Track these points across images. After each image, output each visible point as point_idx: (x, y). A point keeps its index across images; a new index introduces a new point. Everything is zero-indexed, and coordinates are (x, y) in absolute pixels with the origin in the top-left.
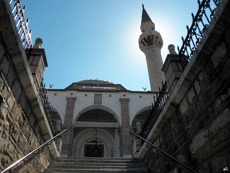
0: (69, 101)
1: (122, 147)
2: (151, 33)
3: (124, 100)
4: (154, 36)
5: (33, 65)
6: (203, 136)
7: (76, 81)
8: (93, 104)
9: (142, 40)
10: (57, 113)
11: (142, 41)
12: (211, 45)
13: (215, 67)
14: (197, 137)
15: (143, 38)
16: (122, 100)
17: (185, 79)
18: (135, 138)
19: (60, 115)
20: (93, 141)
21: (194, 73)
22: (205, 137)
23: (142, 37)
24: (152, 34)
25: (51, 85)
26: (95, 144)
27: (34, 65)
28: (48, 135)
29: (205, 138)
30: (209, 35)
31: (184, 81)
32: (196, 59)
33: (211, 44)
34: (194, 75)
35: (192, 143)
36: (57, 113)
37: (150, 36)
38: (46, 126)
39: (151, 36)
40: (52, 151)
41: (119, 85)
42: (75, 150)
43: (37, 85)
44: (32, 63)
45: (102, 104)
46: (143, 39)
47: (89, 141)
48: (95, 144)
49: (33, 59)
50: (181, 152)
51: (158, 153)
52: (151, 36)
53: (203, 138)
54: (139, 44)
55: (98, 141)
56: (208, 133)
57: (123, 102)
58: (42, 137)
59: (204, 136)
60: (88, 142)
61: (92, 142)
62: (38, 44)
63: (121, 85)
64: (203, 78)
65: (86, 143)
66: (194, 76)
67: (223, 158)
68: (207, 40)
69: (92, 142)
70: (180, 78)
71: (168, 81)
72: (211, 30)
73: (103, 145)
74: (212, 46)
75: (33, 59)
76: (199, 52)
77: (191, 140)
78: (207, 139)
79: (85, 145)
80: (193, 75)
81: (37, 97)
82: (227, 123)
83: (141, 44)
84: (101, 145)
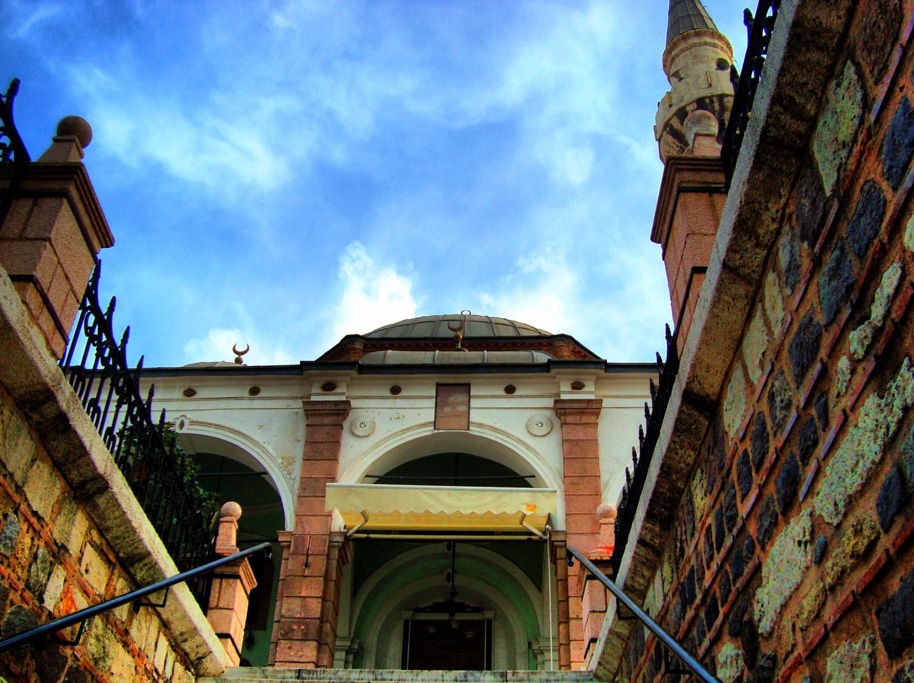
0: (317, 420)
1: (568, 627)
2: (714, 84)
3: (576, 405)
4: (725, 99)
5: (27, 239)
6: (796, 544)
7: (363, 329)
8: (428, 431)
9: (670, 119)
10: (263, 476)
11: (672, 128)
12: (806, 84)
13: (828, 193)
14: (774, 550)
15: (674, 109)
16: (567, 406)
17: (725, 265)
18: (587, 580)
19: (275, 485)
20: (440, 604)
21: (757, 238)
22: (803, 545)
23: (671, 106)
24: (719, 92)
25: (239, 349)
26: (444, 617)
27: (31, 239)
28: (146, 561)
29: (802, 553)
30: (787, 36)
31: (721, 280)
32: (751, 162)
33: (804, 80)
34: (757, 245)
35: (760, 585)
36: (263, 476)
37: (707, 101)
38: (126, 522)
39: (712, 102)
40: (186, 640)
41: (563, 337)
42: (360, 644)
43: (45, 328)
44: (25, 228)
45: (474, 431)
46: (675, 114)
47: (421, 606)
48: (444, 617)
49: (31, 211)
50: (726, 630)
51: (658, 642)
52: (715, 99)
53: (796, 549)
54: (659, 140)
55: (467, 603)
56: (812, 526)
57: (570, 419)
58: (116, 572)
59: (800, 543)
60: (418, 610)
61: (436, 608)
62: (67, 145)
63: (570, 338)
64: (792, 256)
65: (408, 615)
66: (758, 250)
67: (856, 646)
68: (785, 59)
69: (436, 608)
70: (707, 268)
71: (675, 286)
72: (793, 10)
73: (490, 622)
74: (810, 91)
75: (31, 211)
76: (762, 124)
77: (758, 568)
78: (809, 557)
79: (406, 622)
80: (754, 242)
81: (51, 384)
82: (871, 468)
83: (670, 139)
84: (480, 623)
